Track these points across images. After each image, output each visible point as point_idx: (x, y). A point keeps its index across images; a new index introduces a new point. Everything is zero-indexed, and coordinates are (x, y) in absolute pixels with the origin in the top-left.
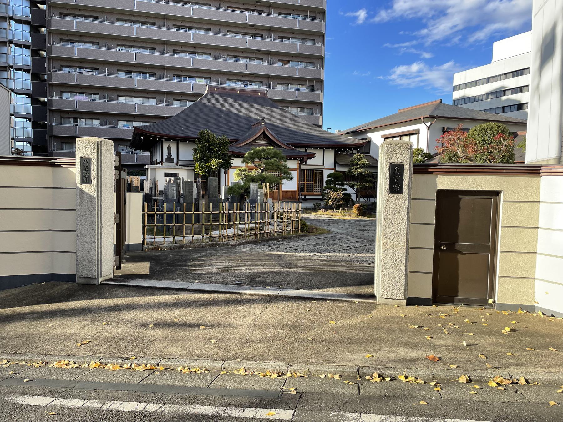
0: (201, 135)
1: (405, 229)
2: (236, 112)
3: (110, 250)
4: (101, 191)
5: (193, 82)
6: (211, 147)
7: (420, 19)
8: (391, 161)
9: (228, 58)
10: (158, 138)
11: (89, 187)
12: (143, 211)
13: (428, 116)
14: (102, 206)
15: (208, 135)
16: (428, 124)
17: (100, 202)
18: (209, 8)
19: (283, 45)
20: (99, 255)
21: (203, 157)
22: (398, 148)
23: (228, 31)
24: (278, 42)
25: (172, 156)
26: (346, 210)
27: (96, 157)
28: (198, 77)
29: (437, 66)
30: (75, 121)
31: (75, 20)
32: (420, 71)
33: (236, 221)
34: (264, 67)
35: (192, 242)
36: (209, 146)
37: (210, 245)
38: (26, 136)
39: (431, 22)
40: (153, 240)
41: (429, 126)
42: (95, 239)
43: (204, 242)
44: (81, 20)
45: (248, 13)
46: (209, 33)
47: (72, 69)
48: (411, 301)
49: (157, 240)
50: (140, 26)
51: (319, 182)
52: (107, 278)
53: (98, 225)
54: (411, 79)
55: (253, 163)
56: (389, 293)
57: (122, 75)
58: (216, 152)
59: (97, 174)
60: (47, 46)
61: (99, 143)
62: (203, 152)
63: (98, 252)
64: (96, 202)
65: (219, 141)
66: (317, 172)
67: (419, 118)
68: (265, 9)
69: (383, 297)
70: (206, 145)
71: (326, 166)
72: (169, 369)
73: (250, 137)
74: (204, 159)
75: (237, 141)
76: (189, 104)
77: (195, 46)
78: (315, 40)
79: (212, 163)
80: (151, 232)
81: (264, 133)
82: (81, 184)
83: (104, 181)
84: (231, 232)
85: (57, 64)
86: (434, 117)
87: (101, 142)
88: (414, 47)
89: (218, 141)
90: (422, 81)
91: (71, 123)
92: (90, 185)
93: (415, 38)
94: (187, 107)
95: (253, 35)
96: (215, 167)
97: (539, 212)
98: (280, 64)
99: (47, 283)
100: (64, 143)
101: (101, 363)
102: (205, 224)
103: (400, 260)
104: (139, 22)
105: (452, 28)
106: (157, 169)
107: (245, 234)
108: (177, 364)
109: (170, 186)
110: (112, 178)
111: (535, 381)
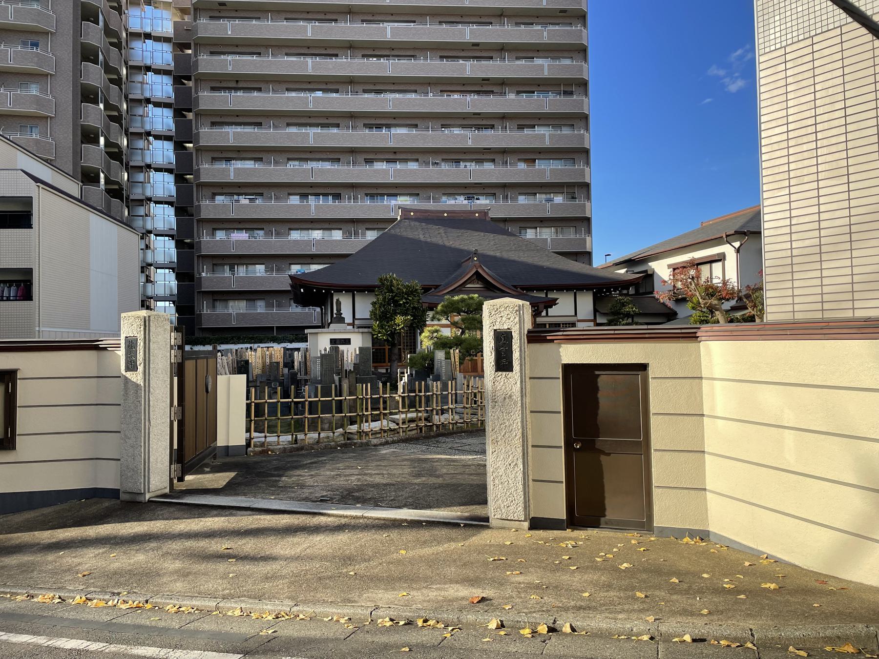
0: (381, 282)
1: (519, 420)
3: (163, 456)
4: (149, 380)
6: (396, 298)
8: (495, 328)
9: (443, 164)
11: (134, 375)
12: (247, 399)
13: (733, 232)
14: (151, 399)
16: (737, 244)
17: (147, 393)
18: (413, 96)
19: (524, 138)
20: (147, 462)
22: (503, 309)
23: (442, 125)
24: (517, 134)
27: (143, 336)
28: (401, 195)
30: (232, 269)
31: (231, 130)
33: (467, 403)
35: (318, 442)
36: (393, 297)
37: (342, 446)
38: (168, 292)
40: (263, 439)
41: (739, 248)
42: (141, 442)
43: (334, 441)
44: (239, 130)
45: (469, 98)
46: (414, 131)
47: (227, 197)
48: (536, 524)
49: (268, 439)
50: (318, 130)
52: (159, 493)
53: (145, 423)
55: (447, 319)
56: (503, 511)
57: (295, 200)
60: (194, 168)
61: (147, 319)
62: (384, 306)
63: (145, 459)
65: (407, 289)
67: (721, 235)
68: (495, 89)
69: (496, 517)
71: (579, 317)
72: (157, 608)
73: (456, 280)
75: (437, 287)
76: (371, 235)
77: (395, 151)
81: (477, 273)
84: (376, 426)
85: (207, 192)
86: (744, 234)
87: (149, 317)
89: (404, 290)
91: (227, 273)
95: (479, 127)
96: (401, 327)
97: (702, 393)
98: (522, 166)
99: (87, 501)
100: (217, 300)
101: (87, 598)
103: (516, 464)
104: (316, 125)
106: (319, 335)
107: (399, 428)
108: (168, 601)
110: (167, 362)
111: (584, 630)
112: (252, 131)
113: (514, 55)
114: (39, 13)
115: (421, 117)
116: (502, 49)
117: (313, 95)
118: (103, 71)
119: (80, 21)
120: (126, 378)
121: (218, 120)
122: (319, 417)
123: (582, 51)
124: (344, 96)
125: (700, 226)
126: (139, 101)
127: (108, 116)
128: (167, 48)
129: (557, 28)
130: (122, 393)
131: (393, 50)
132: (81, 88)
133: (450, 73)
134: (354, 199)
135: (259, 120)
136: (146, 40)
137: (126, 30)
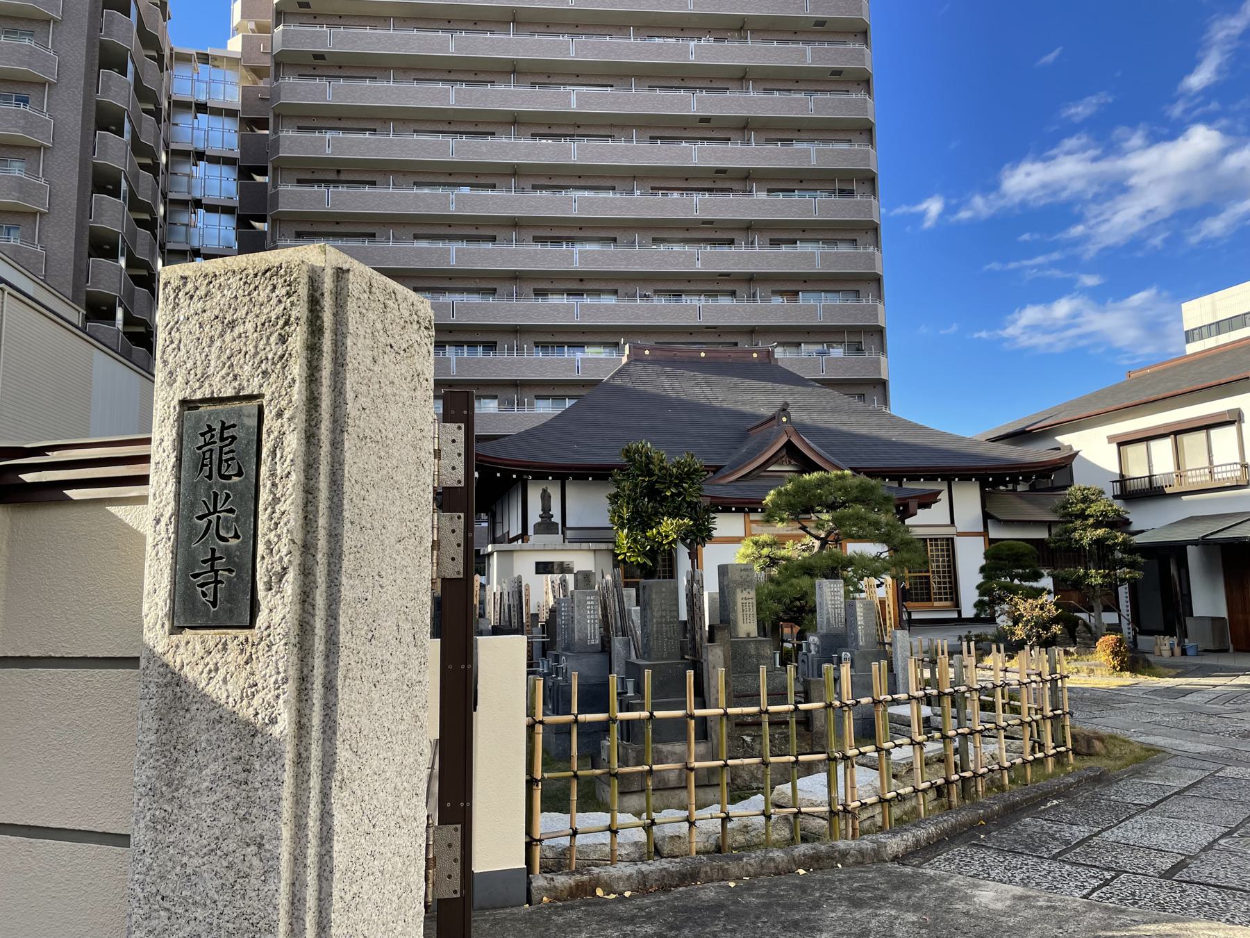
0: (627, 457)
2: (703, 401)
4: (330, 687)
5: (579, 355)
6: (657, 486)
7: (1069, 204)
10: (515, 472)
11: (233, 655)
14: (339, 818)
15: (647, 457)
17: (315, 782)
21: (636, 513)
24: (770, 252)
25: (552, 516)
26: (1072, 654)
27: (298, 393)
29: (1114, 301)
32: (1075, 315)
34: (740, 310)
36: (651, 484)
39: (1094, 209)
45: (697, 197)
46: (612, 247)
50: (464, 245)
51: (944, 572)
54: (1054, 335)
58: (670, 499)
59: (298, 537)
61: (328, 284)
62: (634, 500)
64: (287, 792)
66: (937, 545)
68: (735, 186)
70: (644, 481)
71: (961, 526)
73: (752, 455)
74: (641, 521)
75: (717, 469)
77: (581, 277)
78: (855, 240)
79: (662, 529)
80: (556, 801)
81: (789, 446)
82: (176, 630)
83: (359, 592)
87: (340, 273)
88: (1054, 265)
90: (1081, 337)
92: (242, 634)
93: (1054, 247)
94: (567, 407)
98: (777, 301)
102: (773, 759)
105: (1143, 217)
106: (515, 554)
109: (579, 601)
112: (360, 244)
113: (764, 135)
114: (32, 52)
115: (622, 227)
116: (745, 127)
117: (456, 192)
118: (126, 208)
119: (97, 69)
120: (173, 681)
121: (308, 228)
122: (726, 765)
123: (866, 130)
124: (504, 194)
125: (1126, 378)
126: (184, 203)
127: (131, 276)
128: (231, 125)
129: (828, 96)
130: (144, 775)
131: (578, 127)
132: (94, 171)
133: (668, 161)
134: (517, 350)
135: (370, 230)
136: (198, 115)
137: (170, 98)
